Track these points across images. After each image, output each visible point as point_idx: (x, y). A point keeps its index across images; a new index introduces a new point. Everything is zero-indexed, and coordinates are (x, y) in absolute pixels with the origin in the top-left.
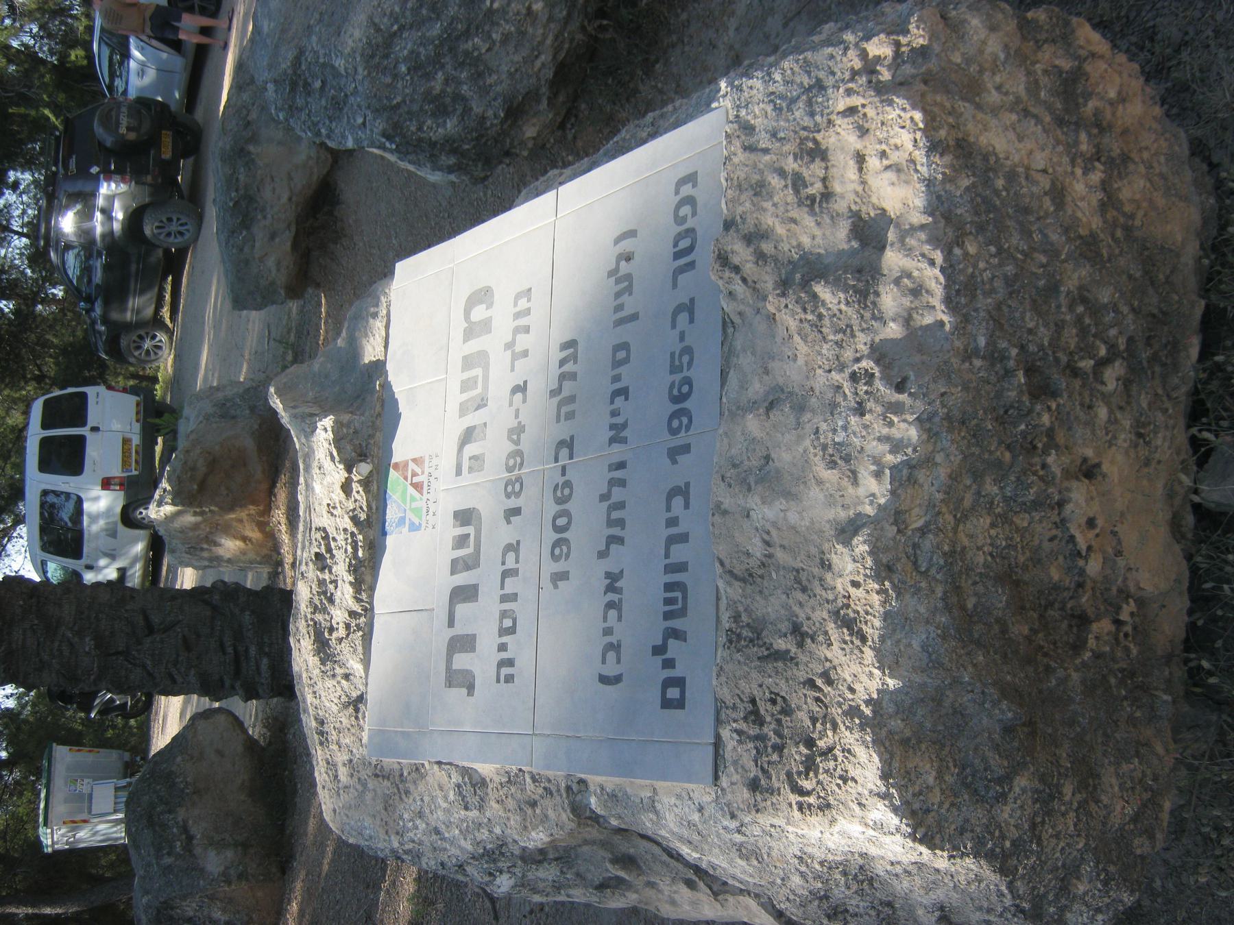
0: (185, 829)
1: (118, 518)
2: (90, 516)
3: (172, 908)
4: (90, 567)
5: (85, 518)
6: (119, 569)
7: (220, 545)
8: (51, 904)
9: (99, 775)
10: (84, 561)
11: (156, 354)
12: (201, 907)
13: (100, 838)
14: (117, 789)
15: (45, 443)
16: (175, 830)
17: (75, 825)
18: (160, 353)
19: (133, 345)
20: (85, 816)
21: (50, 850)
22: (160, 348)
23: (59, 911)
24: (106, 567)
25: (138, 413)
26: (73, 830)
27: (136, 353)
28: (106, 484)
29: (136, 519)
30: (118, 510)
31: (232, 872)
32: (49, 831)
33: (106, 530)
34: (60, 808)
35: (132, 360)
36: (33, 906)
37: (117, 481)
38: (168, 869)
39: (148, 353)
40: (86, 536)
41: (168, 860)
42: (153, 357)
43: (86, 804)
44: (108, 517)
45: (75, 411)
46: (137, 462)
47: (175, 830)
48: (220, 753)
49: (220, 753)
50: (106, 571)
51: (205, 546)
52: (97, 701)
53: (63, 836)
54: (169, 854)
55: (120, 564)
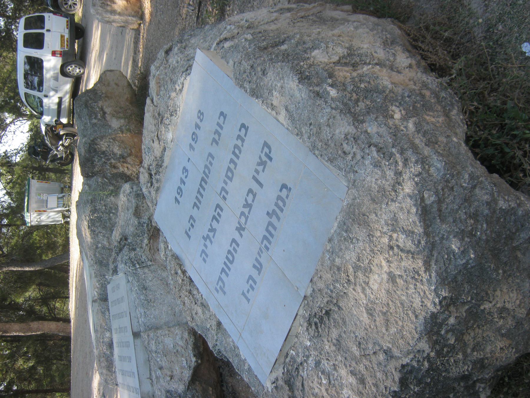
0: (102, 109)
1: (59, 71)
2: (46, 70)
3: (96, 144)
4: (46, 96)
5: (44, 70)
6: (59, 98)
7: (116, 3)
8: (29, 266)
9: (50, 192)
10: (43, 93)
11: (74, 7)
12: (109, 145)
13: (51, 220)
14: (58, 198)
15: (26, 36)
16: (98, 109)
17: (40, 212)
18: (76, 7)
19: (64, 3)
20: (44, 209)
21: (29, 225)
22: (76, 4)
23: (32, 269)
24: (53, 96)
25: (67, 25)
26: (39, 215)
27: (65, 6)
28: (54, 54)
29: (67, 72)
30: (59, 66)
31: (123, 128)
32: (29, 214)
33: (54, 77)
34: (33, 205)
35: (63, 9)
36: (21, 267)
37: (59, 52)
38: (95, 125)
39: (70, 6)
40: (44, 80)
41: (94, 121)
42: (73, 8)
43: (45, 204)
44: (55, 70)
45: (40, 22)
46: (67, 45)
47: (98, 109)
48: (117, 85)
49: (117, 85)
50: (53, 98)
51: (109, 3)
52: (50, 155)
53: (35, 218)
54: (95, 118)
55: (60, 95)
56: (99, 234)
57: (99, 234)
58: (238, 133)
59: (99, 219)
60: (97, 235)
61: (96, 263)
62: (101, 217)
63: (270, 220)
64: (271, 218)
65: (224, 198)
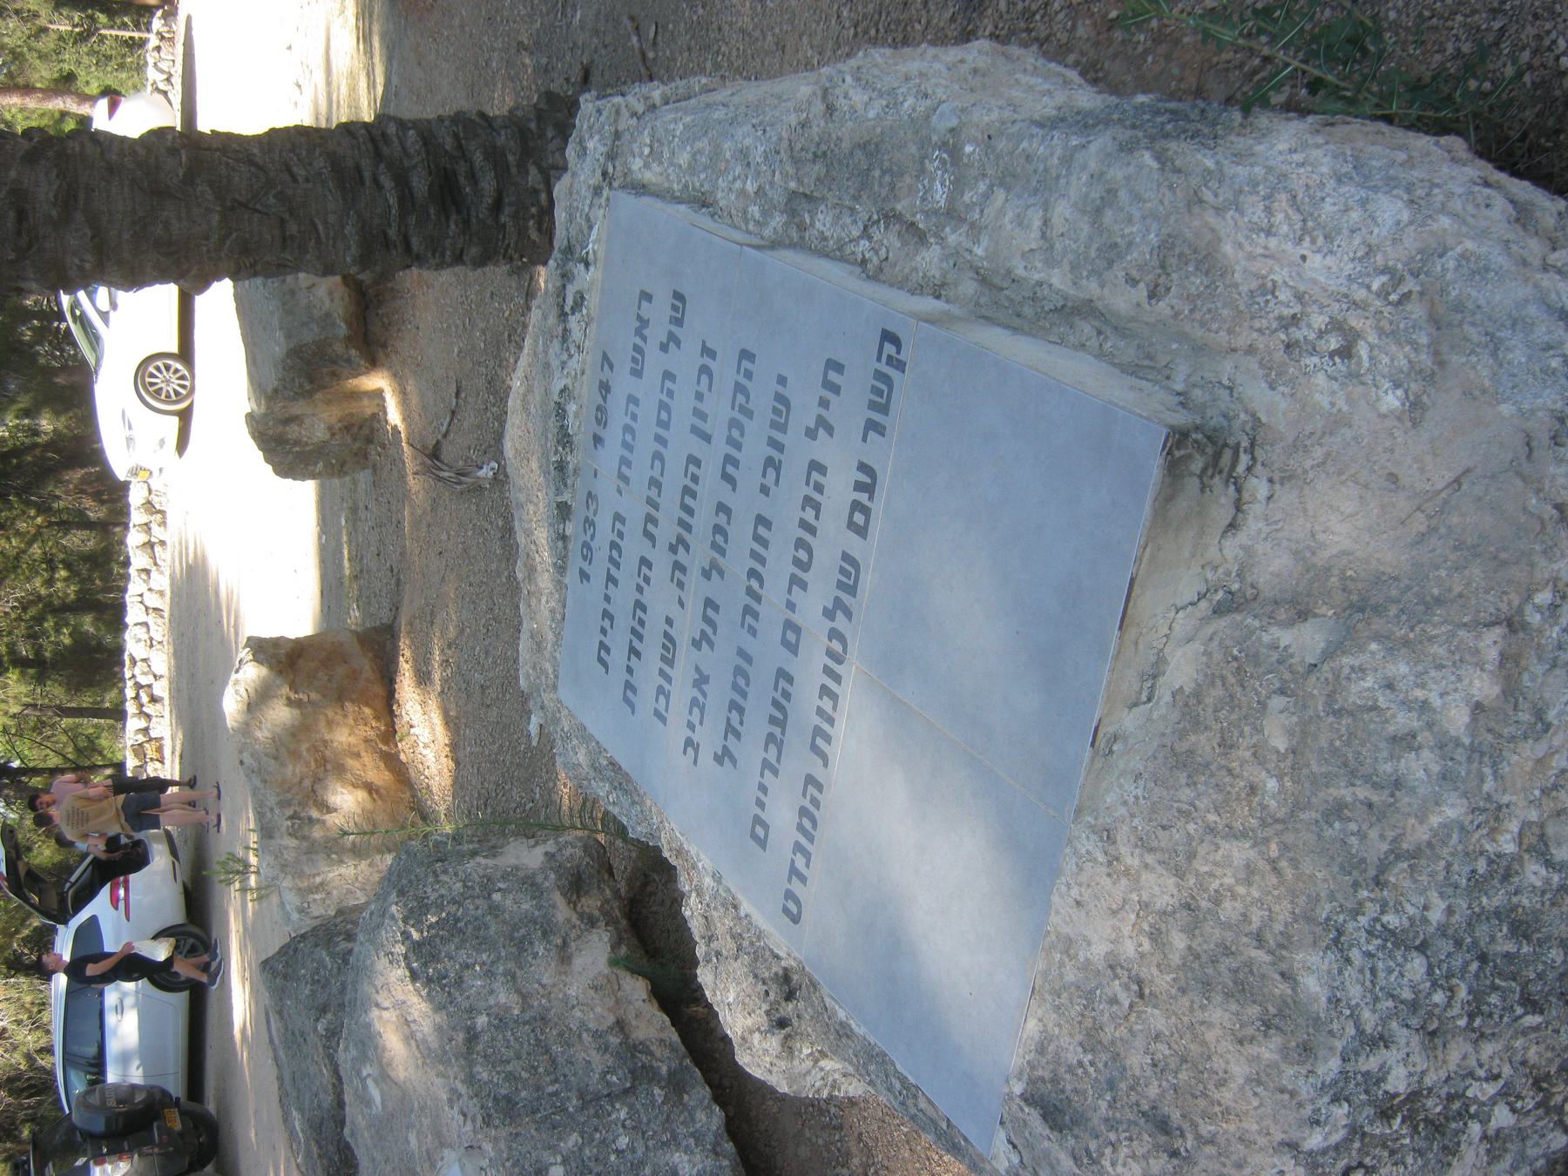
51: (315, 814)
56: (467, 974)
57: (467, 974)
58: (764, 755)
59: (451, 927)
60: (459, 981)
61: (487, 1121)
62: (457, 920)
63: (833, 625)
64: (833, 620)
65: (753, 631)
